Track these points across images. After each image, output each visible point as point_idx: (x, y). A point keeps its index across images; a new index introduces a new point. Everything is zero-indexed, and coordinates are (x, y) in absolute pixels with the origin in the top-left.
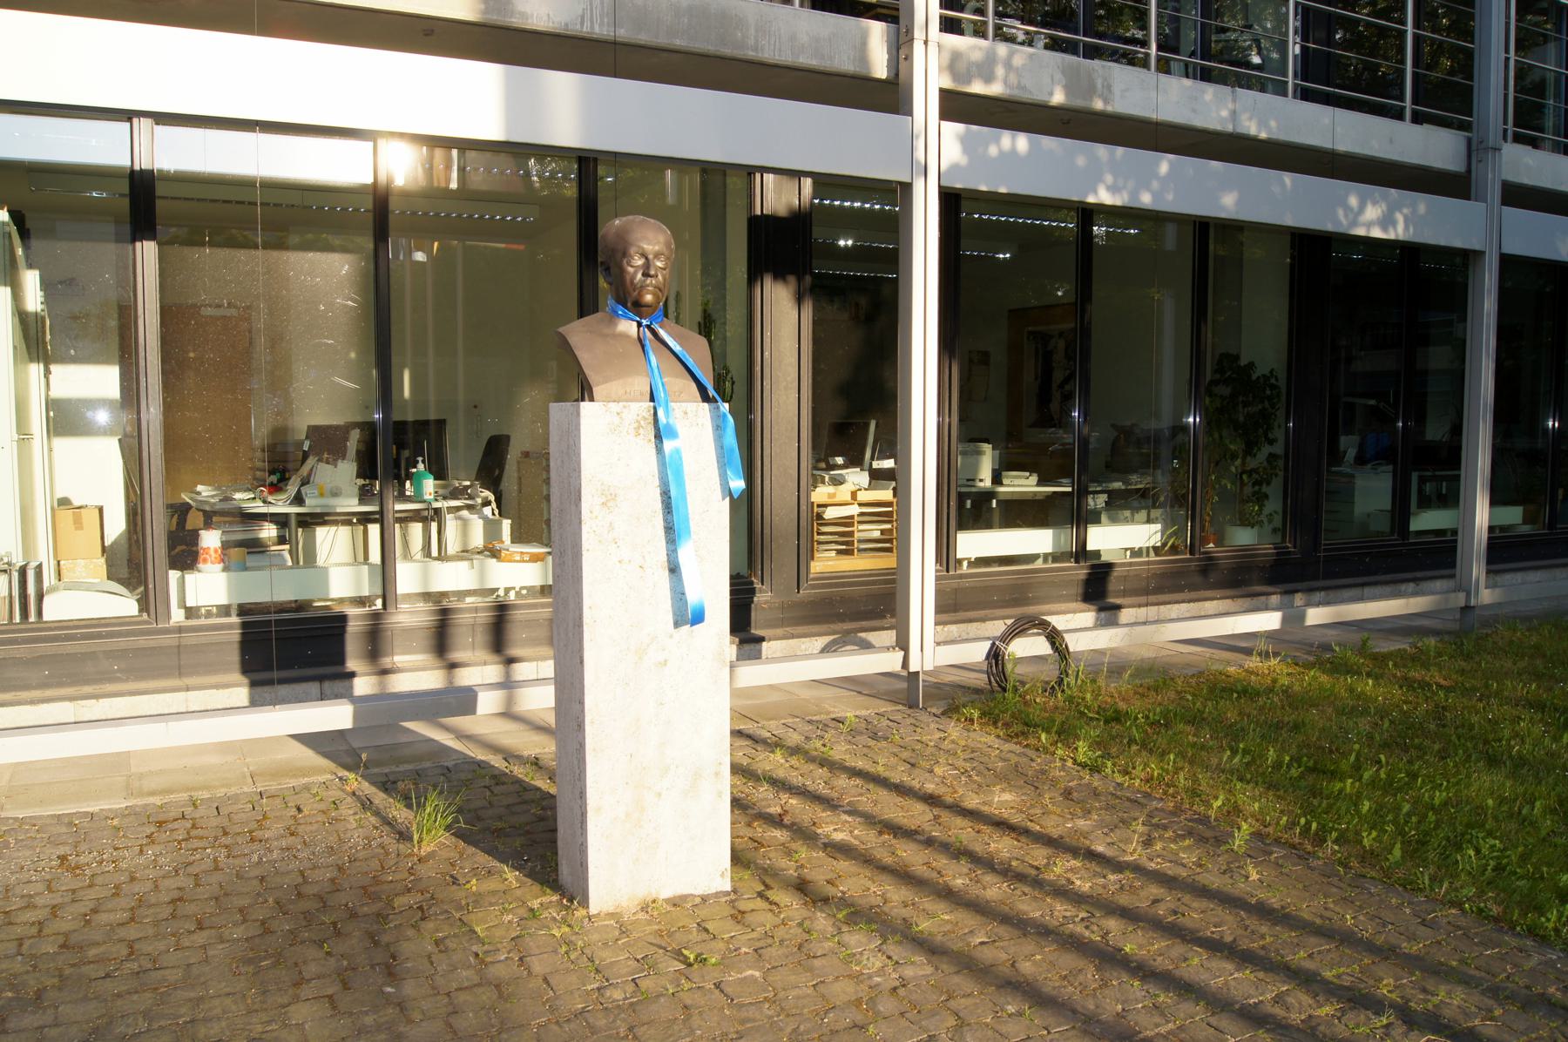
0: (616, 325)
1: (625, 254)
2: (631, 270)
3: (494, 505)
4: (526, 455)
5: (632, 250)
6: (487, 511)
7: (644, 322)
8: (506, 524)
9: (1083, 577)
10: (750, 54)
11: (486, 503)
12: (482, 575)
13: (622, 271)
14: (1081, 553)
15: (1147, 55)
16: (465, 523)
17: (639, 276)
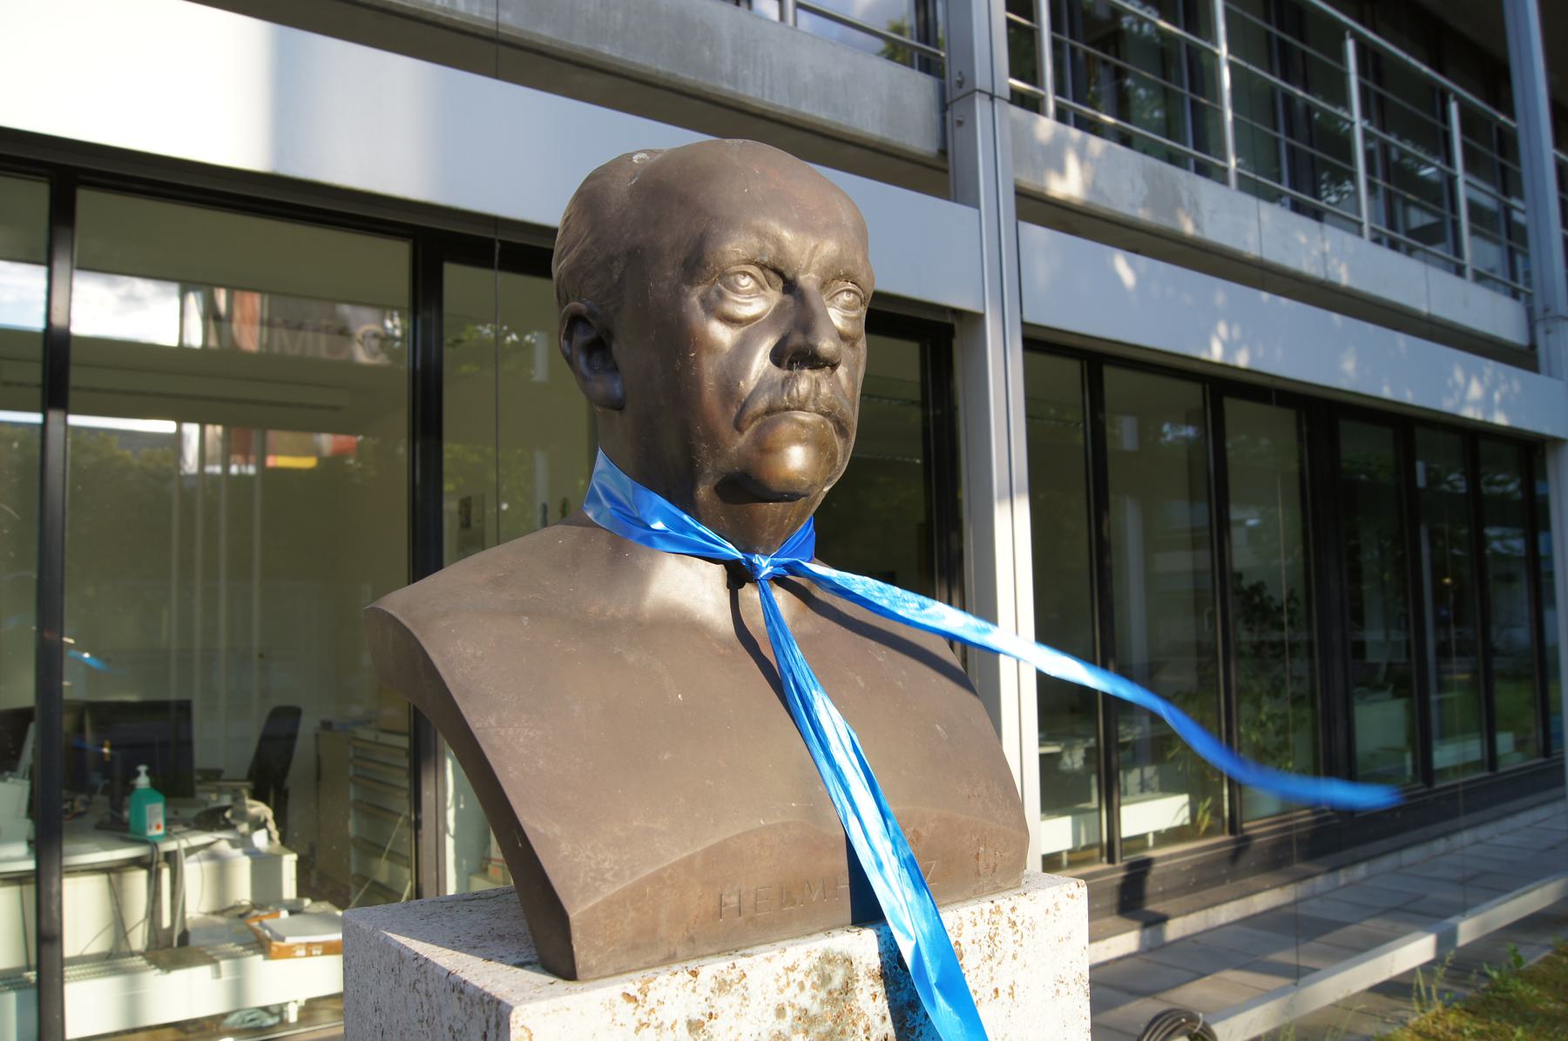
0: (641, 578)
1: (697, 263)
2: (723, 335)
3: (272, 825)
4: (327, 725)
5: (736, 247)
6: (260, 839)
7: (765, 565)
8: (289, 862)
9: (1118, 882)
10: (726, 87)
11: (259, 824)
12: (238, 988)
13: (677, 344)
14: (1111, 848)
15: (1225, 170)
16: (221, 866)
17: (760, 363)
